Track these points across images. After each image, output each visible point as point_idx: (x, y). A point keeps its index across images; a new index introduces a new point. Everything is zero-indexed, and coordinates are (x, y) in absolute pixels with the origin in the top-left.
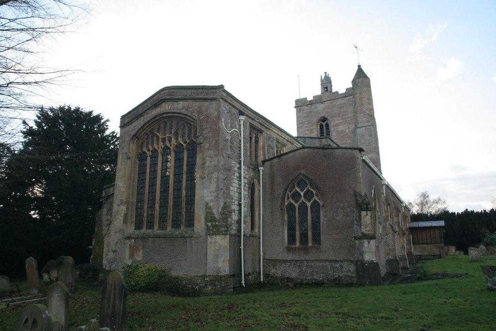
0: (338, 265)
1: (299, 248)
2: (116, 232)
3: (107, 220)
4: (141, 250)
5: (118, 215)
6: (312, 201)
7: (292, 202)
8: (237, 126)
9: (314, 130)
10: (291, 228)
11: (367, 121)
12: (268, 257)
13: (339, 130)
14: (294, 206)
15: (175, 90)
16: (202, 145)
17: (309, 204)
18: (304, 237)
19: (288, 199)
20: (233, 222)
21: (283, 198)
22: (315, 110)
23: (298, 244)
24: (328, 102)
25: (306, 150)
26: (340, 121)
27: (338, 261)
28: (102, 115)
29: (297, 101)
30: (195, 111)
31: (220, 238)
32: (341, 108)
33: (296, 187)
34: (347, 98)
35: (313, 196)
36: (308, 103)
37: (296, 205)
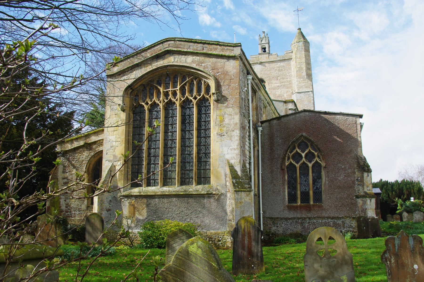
0: (340, 222)
1: (300, 206)
3: (64, 179)
6: (313, 162)
7: (292, 162)
10: (292, 186)
12: (267, 215)
14: (295, 167)
15: (182, 43)
17: (310, 165)
18: (305, 196)
19: (289, 159)
21: (284, 159)
23: (299, 203)
25: (307, 113)
26: (278, 85)
27: (340, 218)
30: (210, 67)
31: (245, 195)
33: (297, 148)
35: (315, 158)
37: (298, 166)
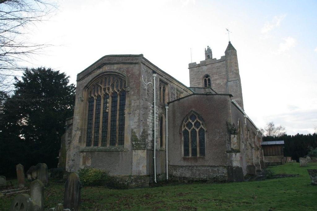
0: (216, 169)
1: (191, 158)
2: (74, 148)
3: (69, 141)
4: (90, 160)
5: (76, 137)
6: (199, 128)
7: (187, 129)
8: (152, 81)
9: (201, 83)
10: (186, 146)
11: (235, 77)
12: (171, 164)
13: (217, 83)
14: (188, 132)
15: (112, 57)
16: (129, 92)
17: (197, 130)
18: (194, 151)
19: (184, 127)
20: (149, 141)
21: (181, 127)
22: (201, 70)
23: (190, 156)
24: (210, 65)
25: (195, 96)
26: (217, 77)
27: (216, 166)
28: (65, 73)
29: (190, 65)
30: (125, 71)
31: (141, 152)
32: (218, 69)
33: (189, 119)
34: (222, 63)
35: (200, 125)
36: (197, 66)
37: (189, 131)
